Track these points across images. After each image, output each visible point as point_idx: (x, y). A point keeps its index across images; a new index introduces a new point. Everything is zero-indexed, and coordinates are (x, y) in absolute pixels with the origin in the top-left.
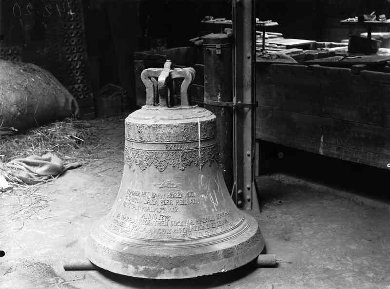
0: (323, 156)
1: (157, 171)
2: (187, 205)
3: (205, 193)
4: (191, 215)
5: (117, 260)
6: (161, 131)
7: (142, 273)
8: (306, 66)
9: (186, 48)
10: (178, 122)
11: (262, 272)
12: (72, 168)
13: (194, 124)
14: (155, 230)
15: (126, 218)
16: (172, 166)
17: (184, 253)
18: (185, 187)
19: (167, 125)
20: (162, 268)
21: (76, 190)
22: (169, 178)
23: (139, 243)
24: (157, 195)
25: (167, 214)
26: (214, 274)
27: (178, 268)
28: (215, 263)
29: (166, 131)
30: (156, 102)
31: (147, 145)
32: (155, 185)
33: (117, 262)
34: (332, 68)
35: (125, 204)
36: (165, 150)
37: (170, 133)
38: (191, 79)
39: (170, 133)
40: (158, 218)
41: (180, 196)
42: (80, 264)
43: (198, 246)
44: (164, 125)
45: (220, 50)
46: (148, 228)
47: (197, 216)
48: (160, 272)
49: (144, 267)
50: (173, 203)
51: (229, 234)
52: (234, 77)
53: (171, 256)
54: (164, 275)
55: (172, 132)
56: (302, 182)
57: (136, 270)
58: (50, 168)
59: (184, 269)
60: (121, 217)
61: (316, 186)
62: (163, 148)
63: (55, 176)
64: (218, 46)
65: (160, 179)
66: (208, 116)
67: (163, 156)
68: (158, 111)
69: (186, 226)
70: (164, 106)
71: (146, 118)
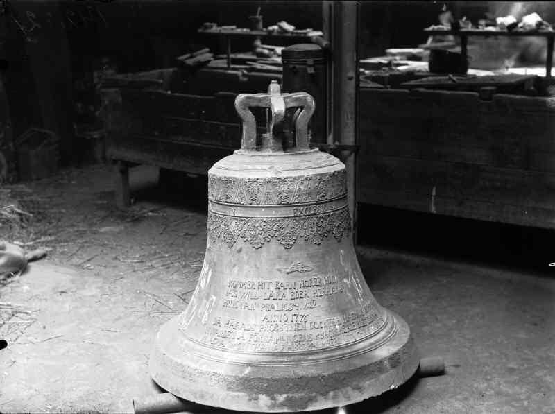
0: (435, 215)
1: (282, 248)
2: (329, 297)
3: (347, 276)
4: (334, 310)
5: (238, 391)
6: (286, 187)
7: (282, 405)
8: (407, 91)
9: (171, 70)
10: (310, 173)
11: (429, 384)
12: (34, 259)
13: (329, 175)
14: (289, 338)
15: (235, 324)
16: (303, 239)
17: (339, 368)
18: (323, 270)
19: (295, 178)
20: (314, 394)
21: (63, 292)
22: (299, 258)
23: (267, 360)
24: (284, 284)
25: (303, 312)
26: (383, 393)
27: (336, 391)
28: (383, 376)
29: (295, 187)
30: (259, 145)
31: (263, 210)
32: (279, 270)
33: (236, 394)
34: (448, 92)
35: (227, 303)
36: (293, 215)
37: (299, 190)
38: (313, 109)
39: (299, 190)
40: (290, 319)
41: (318, 284)
42: (161, 404)
43: (355, 355)
44: (291, 177)
45: (313, 68)
46: (276, 336)
47: (343, 311)
48: (312, 400)
49: (285, 396)
50: (309, 295)
51: (384, 337)
52: (330, 107)
53: (324, 374)
54: (318, 404)
55: (302, 188)
56: (391, 255)
57: (273, 401)
58: (8, 261)
59: (344, 390)
60: (222, 324)
61: (416, 259)
62: (290, 212)
63: (16, 273)
64: (310, 61)
65: (286, 260)
66: (334, 165)
67: (290, 226)
68: (273, 158)
69: (332, 328)
70: (279, 150)
71: (240, 169)
